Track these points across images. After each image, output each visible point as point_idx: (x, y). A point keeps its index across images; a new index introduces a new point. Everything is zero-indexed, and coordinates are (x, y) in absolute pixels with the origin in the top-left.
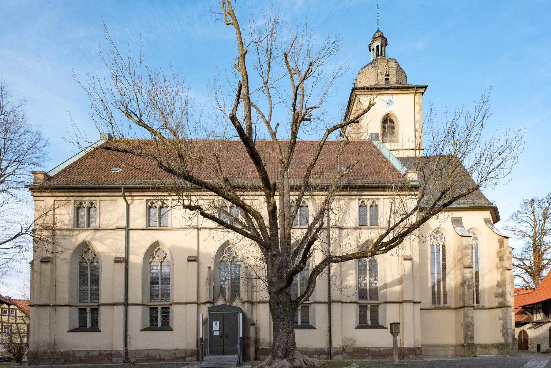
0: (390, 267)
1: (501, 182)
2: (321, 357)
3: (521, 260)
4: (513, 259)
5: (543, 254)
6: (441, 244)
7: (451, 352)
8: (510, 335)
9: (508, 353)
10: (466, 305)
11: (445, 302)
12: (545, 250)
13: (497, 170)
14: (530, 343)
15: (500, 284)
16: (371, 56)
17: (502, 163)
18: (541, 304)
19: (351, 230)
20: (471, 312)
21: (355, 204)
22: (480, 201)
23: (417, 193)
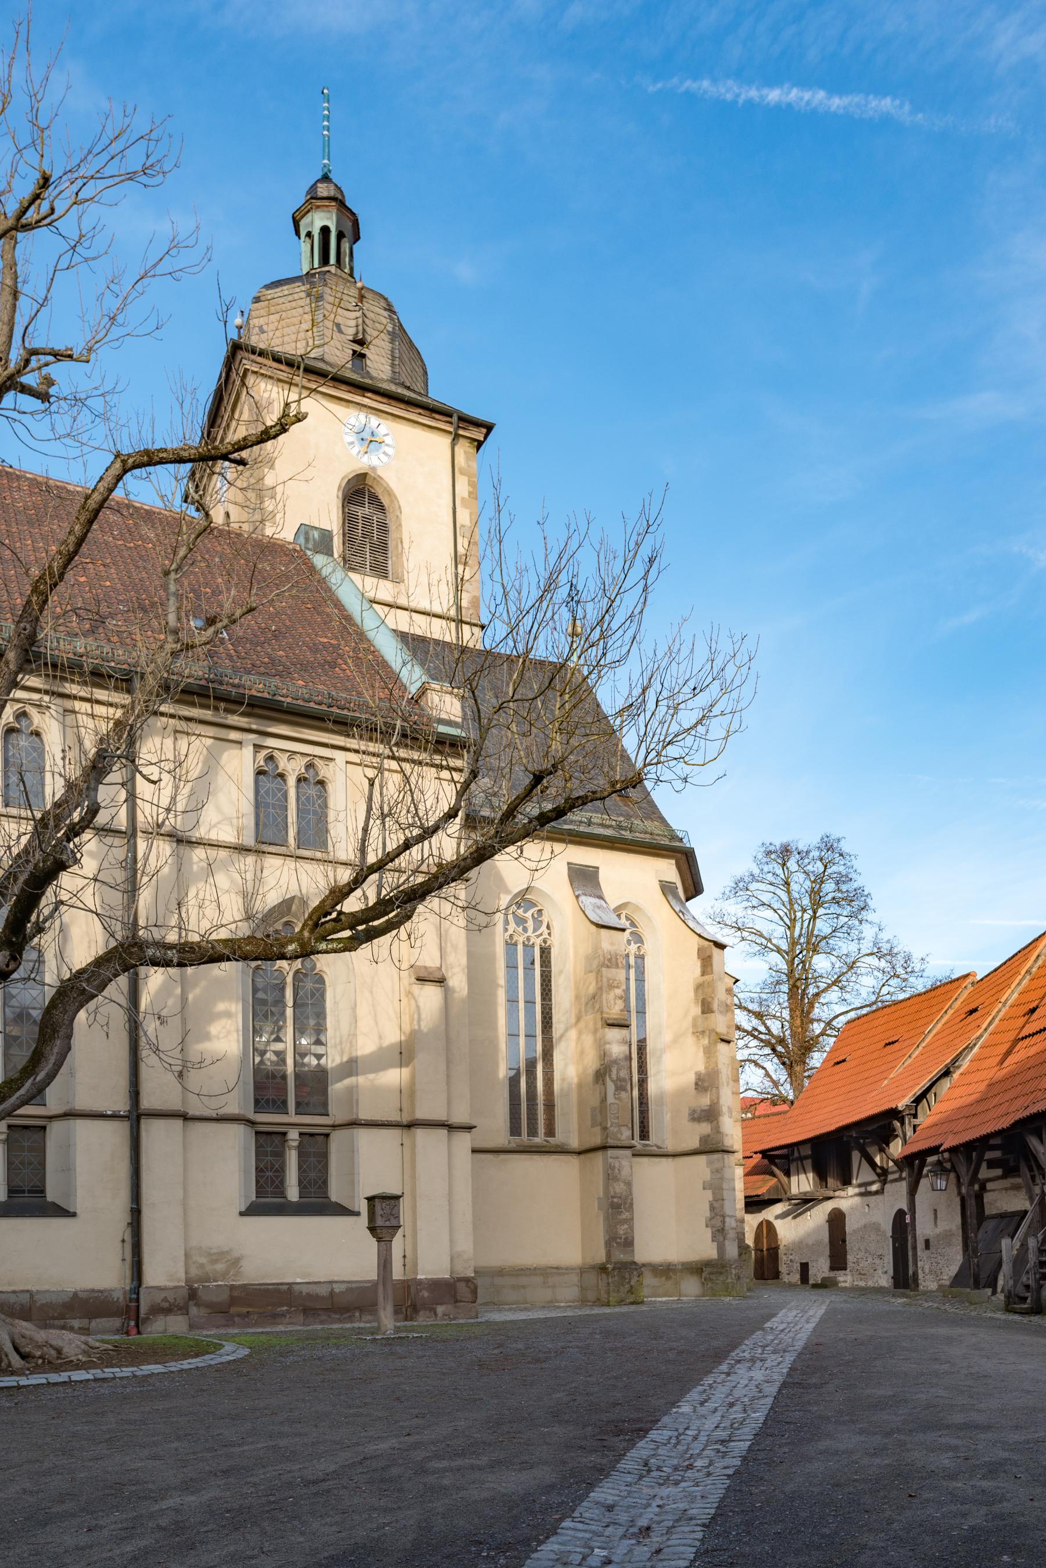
0: (371, 1003)
1: (700, 776)
2: (95, 1324)
3: (759, 1016)
4: (737, 1011)
5: (811, 1005)
6: (538, 942)
7: (568, 1292)
8: (732, 1234)
9: (727, 1290)
10: (611, 1142)
11: (550, 1132)
12: (817, 995)
13: (689, 740)
14: (783, 1258)
15: (705, 1083)
16: (303, 257)
17: (700, 722)
18: (809, 1146)
19: (223, 853)
20: (625, 1163)
21: (239, 763)
22: (649, 825)
23: (458, 763)
